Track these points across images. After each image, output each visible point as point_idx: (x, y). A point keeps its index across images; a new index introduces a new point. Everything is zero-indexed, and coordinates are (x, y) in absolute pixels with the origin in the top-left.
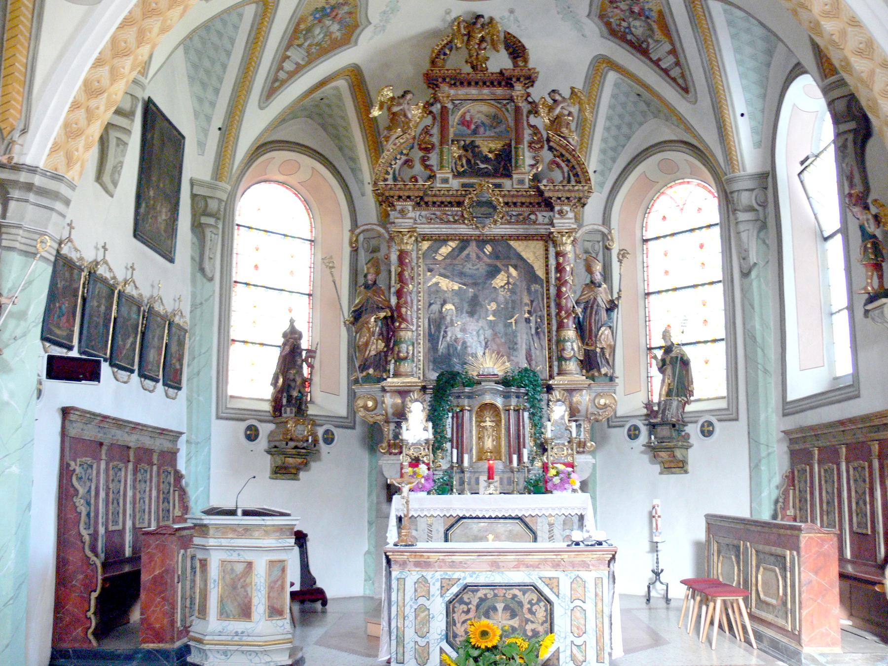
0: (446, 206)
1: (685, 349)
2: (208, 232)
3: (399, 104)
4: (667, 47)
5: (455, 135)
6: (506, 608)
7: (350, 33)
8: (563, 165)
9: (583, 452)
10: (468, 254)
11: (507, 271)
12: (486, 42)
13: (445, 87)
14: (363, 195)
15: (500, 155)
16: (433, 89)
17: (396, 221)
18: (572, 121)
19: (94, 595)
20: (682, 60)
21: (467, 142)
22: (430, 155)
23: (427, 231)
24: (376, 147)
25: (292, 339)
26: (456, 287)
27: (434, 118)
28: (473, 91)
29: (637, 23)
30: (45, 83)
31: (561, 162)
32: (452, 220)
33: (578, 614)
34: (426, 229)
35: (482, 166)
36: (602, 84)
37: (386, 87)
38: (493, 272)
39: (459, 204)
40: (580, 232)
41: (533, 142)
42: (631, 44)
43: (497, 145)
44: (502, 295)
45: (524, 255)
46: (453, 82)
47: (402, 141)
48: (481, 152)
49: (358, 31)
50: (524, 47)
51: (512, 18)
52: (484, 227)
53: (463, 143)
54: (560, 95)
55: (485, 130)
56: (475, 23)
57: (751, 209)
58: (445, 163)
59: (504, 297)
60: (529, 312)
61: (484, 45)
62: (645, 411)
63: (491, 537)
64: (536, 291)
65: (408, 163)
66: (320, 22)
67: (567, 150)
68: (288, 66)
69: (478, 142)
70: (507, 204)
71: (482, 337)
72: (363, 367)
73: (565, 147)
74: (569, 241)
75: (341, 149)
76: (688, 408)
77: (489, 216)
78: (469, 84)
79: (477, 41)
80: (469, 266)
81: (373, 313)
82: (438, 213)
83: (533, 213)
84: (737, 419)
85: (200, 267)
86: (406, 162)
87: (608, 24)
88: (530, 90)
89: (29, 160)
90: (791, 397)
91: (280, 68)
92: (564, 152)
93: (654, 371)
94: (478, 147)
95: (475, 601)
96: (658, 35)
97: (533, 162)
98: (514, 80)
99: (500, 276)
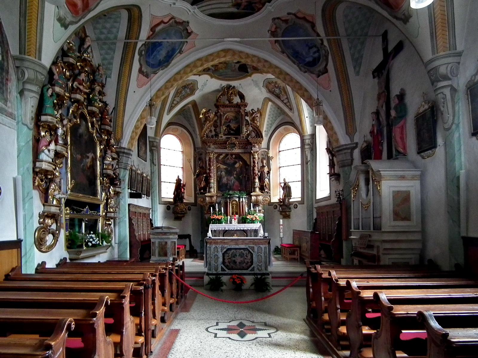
1: (289, 183)
2: (154, 151)
3: (208, 114)
6: (239, 255)
14: (197, 138)
19: (139, 249)
20: (290, 101)
24: (201, 128)
25: (178, 181)
26: (225, 167)
27: (218, 117)
28: (229, 109)
29: (277, 89)
30: (126, 126)
33: (259, 257)
34: (216, 151)
36: (267, 105)
38: (235, 163)
42: (275, 95)
45: (244, 158)
57: (309, 145)
60: (246, 174)
63: (235, 235)
65: (211, 131)
68: (175, 102)
69: (231, 124)
73: (256, 127)
76: (290, 200)
83: (246, 146)
84: (304, 204)
85: (152, 162)
89: (123, 146)
90: (317, 199)
91: (173, 103)
93: (281, 189)
95: (231, 253)
96: (283, 93)
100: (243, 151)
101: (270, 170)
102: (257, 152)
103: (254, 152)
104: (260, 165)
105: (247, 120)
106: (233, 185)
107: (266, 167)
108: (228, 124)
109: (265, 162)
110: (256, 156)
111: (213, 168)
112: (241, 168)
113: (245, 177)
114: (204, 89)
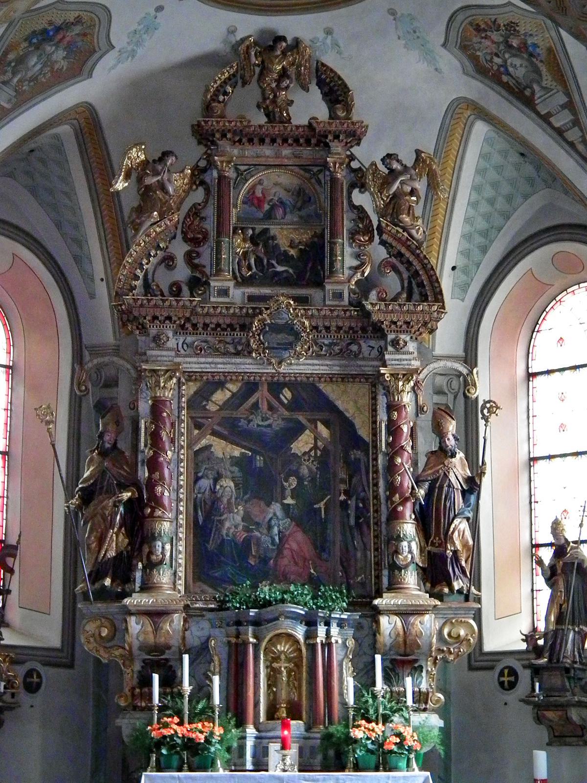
0: (224, 330)
3: (157, 173)
4: (562, 99)
5: (239, 219)
7: (81, 63)
8: (402, 268)
9: (425, 710)
12: (288, 77)
13: (225, 145)
14: (92, 296)
15: (305, 250)
16: (206, 146)
17: (149, 353)
18: (417, 202)
21: (257, 231)
22: (200, 249)
23: (195, 368)
24: (118, 242)
26: (237, 452)
27: (208, 191)
28: (267, 151)
29: (517, 61)
31: (398, 265)
32: (233, 351)
34: (194, 364)
35: (280, 269)
36: (465, 140)
37: (135, 145)
39: (245, 327)
40: (425, 372)
41: (358, 233)
42: (506, 86)
43: (304, 236)
46: (237, 139)
47: (158, 230)
48: (277, 246)
49: (97, 55)
50: (346, 86)
51: (329, 41)
52: (280, 363)
53: (250, 232)
54: (398, 161)
55: (285, 214)
56: (272, 48)
58: (223, 265)
59: (310, 470)
60: (346, 493)
61: (286, 83)
62: (523, 646)
66: (37, 48)
67: (408, 248)
69: (274, 230)
70: (315, 328)
71: (276, 530)
74: (408, 387)
75: (59, 226)
77: (289, 346)
78: (262, 141)
79: (275, 76)
81: (111, 493)
86: (164, 260)
87: (474, 59)
88: (355, 150)
92: (403, 250)
93: (540, 582)
94: (273, 238)
96: (547, 80)
97: (355, 263)
98: (330, 137)
100: (336, 370)
101: (482, 474)
104: (427, 443)
105: (360, 210)
107: (460, 455)
108: (259, 228)
109: (451, 427)
110: (407, 398)
111: (175, 461)
112: (324, 459)
113: (344, 505)
114: (140, 51)
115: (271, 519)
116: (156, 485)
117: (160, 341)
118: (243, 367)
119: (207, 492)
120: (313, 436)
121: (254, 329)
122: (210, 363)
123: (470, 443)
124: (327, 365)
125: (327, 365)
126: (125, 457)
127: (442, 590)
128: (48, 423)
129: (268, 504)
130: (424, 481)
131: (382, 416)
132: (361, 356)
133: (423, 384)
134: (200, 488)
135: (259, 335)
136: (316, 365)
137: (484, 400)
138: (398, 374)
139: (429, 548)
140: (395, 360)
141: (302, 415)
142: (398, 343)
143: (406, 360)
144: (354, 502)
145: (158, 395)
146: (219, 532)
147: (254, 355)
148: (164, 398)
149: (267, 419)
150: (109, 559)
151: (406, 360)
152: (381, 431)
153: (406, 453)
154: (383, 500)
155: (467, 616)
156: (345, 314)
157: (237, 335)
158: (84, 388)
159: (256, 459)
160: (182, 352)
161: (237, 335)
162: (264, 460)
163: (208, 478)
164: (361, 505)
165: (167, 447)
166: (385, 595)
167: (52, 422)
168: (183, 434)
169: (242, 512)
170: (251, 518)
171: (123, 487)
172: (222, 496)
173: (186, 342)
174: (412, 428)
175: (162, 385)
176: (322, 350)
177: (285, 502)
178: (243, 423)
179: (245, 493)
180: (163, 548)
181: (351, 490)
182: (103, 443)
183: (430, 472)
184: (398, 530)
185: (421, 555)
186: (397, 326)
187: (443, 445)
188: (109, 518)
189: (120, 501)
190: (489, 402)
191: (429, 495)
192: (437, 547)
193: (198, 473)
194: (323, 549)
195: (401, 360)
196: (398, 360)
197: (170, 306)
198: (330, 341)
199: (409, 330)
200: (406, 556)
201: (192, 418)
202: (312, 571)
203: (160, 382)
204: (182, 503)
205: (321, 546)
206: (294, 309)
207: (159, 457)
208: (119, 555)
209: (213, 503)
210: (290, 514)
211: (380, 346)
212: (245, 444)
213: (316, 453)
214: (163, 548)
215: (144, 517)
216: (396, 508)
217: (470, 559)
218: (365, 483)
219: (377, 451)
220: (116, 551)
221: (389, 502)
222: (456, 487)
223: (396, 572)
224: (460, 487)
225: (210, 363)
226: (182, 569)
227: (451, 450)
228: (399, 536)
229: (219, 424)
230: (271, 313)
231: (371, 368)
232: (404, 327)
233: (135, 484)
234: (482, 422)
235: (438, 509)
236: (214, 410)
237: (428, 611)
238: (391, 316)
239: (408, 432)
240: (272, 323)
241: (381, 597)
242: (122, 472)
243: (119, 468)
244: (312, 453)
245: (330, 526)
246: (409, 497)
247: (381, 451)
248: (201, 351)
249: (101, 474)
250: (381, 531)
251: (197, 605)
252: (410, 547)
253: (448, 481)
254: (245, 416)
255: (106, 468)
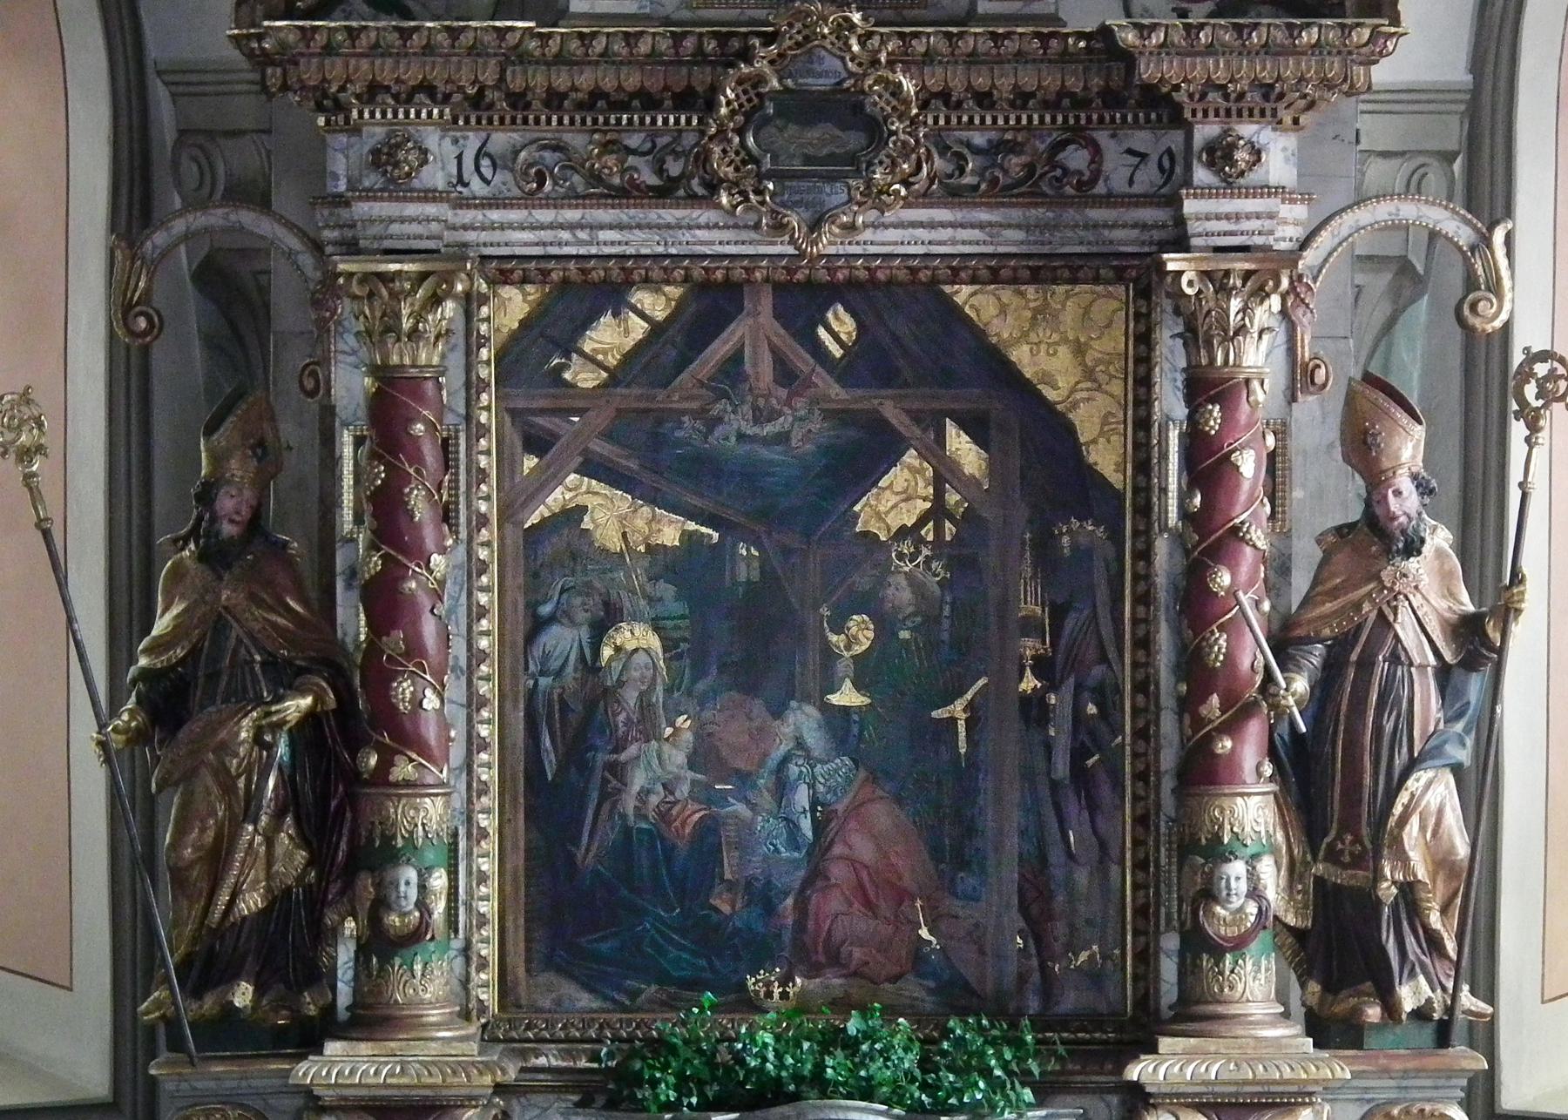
10: (736, 358)
11: (935, 451)
23: (521, 241)
26: (670, 532)
32: (650, 178)
34: (520, 231)
38: (863, 456)
39: (684, 100)
44: (908, 581)
52: (815, 226)
60: (1042, 667)
64: (1083, 555)
71: (802, 797)
72: (207, 968)
77: (853, 164)
80: (739, 421)
81: (244, 698)
82: (576, 140)
83: (1078, 135)
99: (897, 477)
100: (1012, 241)
101: (1507, 612)
102: (1268, 269)
103: (1219, 283)
104: (1326, 496)
106: (816, 875)
107: (1439, 538)
109: (1408, 447)
110: (1258, 357)
111: (459, 589)
112: (963, 543)
113: (1034, 711)
115: (786, 760)
116: (394, 675)
117: (396, 165)
118: (687, 236)
119: (570, 669)
120: (930, 472)
121: (723, 111)
122: (572, 227)
123: (1480, 506)
124: (981, 226)
125: (981, 226)
126: (289, 563)
127: (1357, 1012)
128: (26, 455)
129: (778, 711)
130: (1308, 640)
131: (1170, 402)
132: (1100, 189)
133: (1316, 287)
134: (546, 657)
135: (740, 131)
136: (943, 225)
137: (1527, 350)
138: (1227, 273)
139: (1320, 868)
140: (1218, 217)
141: (892, 398)
142: (1229, 158)
143: (1258, 216)
144: (1069, 698)
145: (395, 359)
146: (614, 806)
147: (724, 200)
148: (413, 372)
149: (773, 415)
150: (244, 918)
151: (1258, 216)
152: (1164, 456)
153: (1248, 550)
154: (1167, 701)
155: (1441, 1093)
156: (1045, 47)
157: (666, 121)
158: (142, 323)
159: (734, 553)
160: (477, 186)
161: (666, 121)
162: (763, 560)
163: (573, 623)
164: (1092, 709)
165: (429, 536)
166: (1165, 1043)
167: (40, 449)
168: (483, 475)
169: (688, 737)
170: (719, 758)
171: (286, 679)
172: (620, 683)
173: (490, 148)
174: (1272, 456)
175: (406, 324)
176: (962, 171)
177: (835, 699)
178: (689, 428)
179: (699, 673)
180: (422, 887)
181: (1060, 658)
182: (214, 519)
183: (1329, 607)
184: (1214, 821)
185: (1290, 886)
186: (1226, 97)
187: (1379, 511)
188: (241, 783)
189: (276, 727)
190: (1544, 356)
191: (1325, 686)
192: (1345, 867)
193: (538, 603)
194: (962, 863)
195: (1237, 217)
196: (1228, 217)
197: (429, 49)
198: (993, 135)
199: (1268, 106)
200: (1241, 909)
201: (513, 412)
202: (924, 933)
203: (398, 316)
204: (485, 714)
205: (953, 847)
206: (864, 39)
207: (404, 578)
208: (279, 901)
209: (591, 705)
210: (852, 741)
211: (1169, 151)
212: (695, 501)
213: (939, 530)
214: (422, 887)
215: (354, 777)
216: (1209, 740)
217: (1459, 901)
218: (1107, 631)
219: (1149, 525)
220: (269, 889)
221: (1187, 719)
222: (1417, 660)
223: (1206, 961)
224: (1432, 660)
225: (572, 227)
226: (491, 931)
227: (1403, 532)
228: (1217, 838)
229: (608, 436)
230: (780, 55)
231: (1134, 233)
232: (1254, 97)
233: (328, 661)
234: (1518, 430)
235: (1353, 745)
236: (590, 385)
237: (1310, 1094)
238: (1205, 65)
239: (1256, 476)
240: (787, 90)
241: (1153, 1049)
242: (281, 621)
243: (271, 609)
244: (928, 532)
245: (987, 784)
246: (1256, 703)
247: (1164, 528)
248: (541, 184)
249: (208, 629)
250: (1158, 806)
251: (542, 1061)
252: (1252, 875)
253: (1390, 641)
254: (695, 405)
255: (226, 608)
